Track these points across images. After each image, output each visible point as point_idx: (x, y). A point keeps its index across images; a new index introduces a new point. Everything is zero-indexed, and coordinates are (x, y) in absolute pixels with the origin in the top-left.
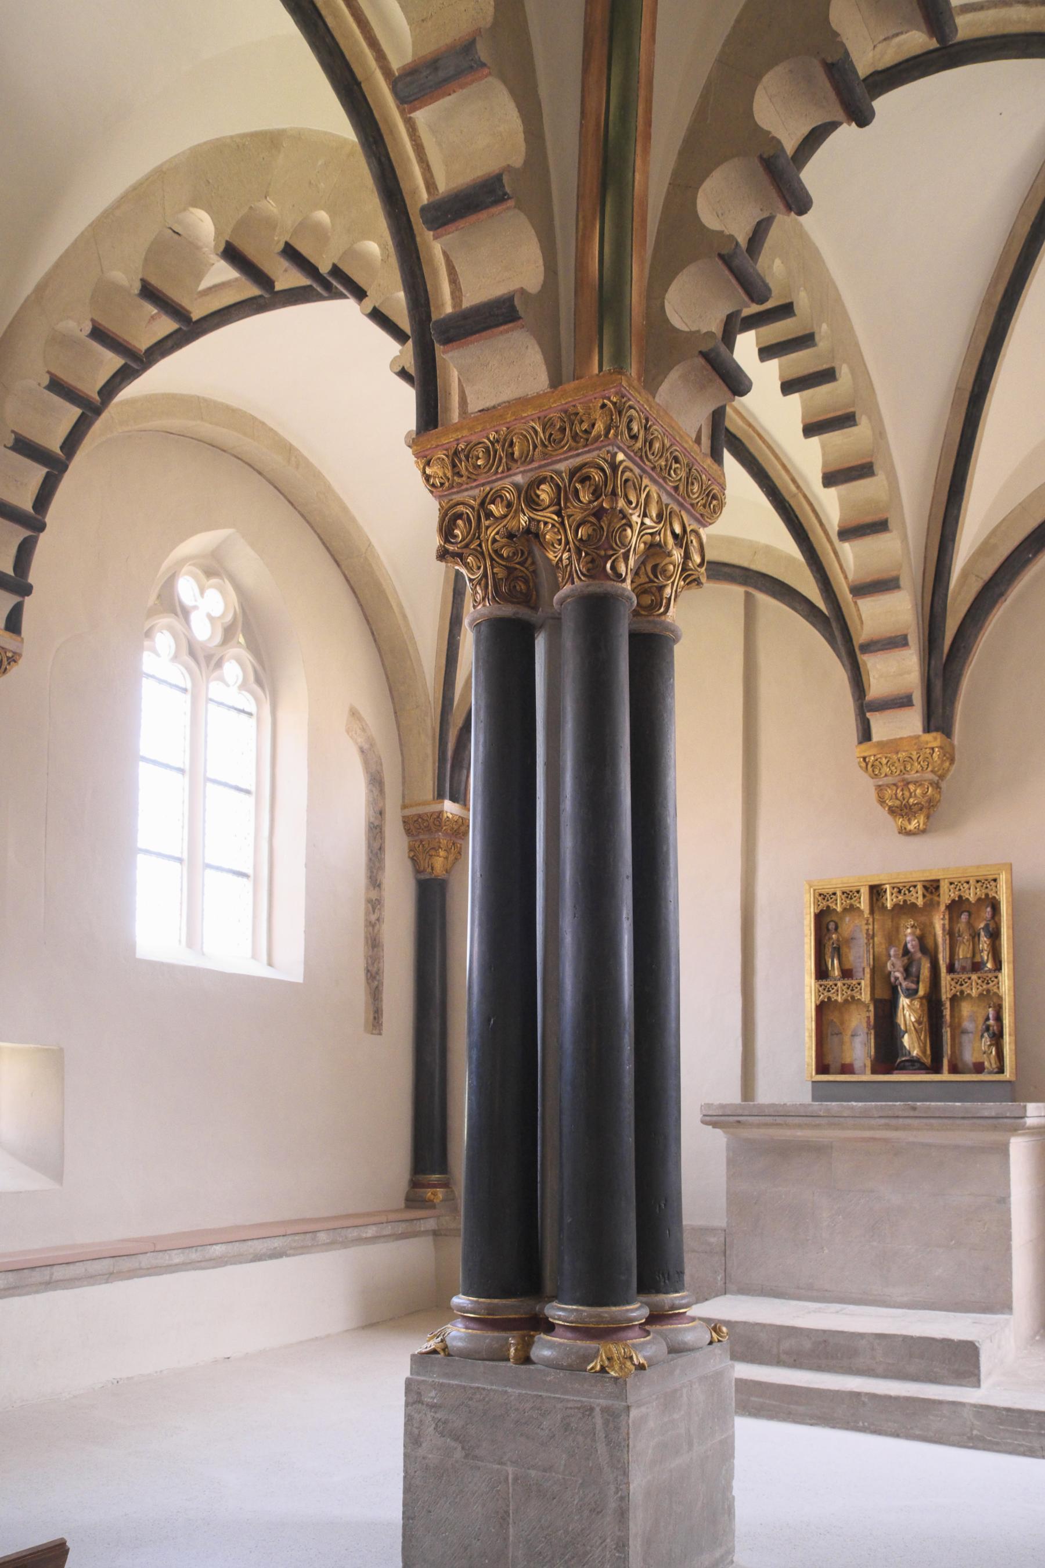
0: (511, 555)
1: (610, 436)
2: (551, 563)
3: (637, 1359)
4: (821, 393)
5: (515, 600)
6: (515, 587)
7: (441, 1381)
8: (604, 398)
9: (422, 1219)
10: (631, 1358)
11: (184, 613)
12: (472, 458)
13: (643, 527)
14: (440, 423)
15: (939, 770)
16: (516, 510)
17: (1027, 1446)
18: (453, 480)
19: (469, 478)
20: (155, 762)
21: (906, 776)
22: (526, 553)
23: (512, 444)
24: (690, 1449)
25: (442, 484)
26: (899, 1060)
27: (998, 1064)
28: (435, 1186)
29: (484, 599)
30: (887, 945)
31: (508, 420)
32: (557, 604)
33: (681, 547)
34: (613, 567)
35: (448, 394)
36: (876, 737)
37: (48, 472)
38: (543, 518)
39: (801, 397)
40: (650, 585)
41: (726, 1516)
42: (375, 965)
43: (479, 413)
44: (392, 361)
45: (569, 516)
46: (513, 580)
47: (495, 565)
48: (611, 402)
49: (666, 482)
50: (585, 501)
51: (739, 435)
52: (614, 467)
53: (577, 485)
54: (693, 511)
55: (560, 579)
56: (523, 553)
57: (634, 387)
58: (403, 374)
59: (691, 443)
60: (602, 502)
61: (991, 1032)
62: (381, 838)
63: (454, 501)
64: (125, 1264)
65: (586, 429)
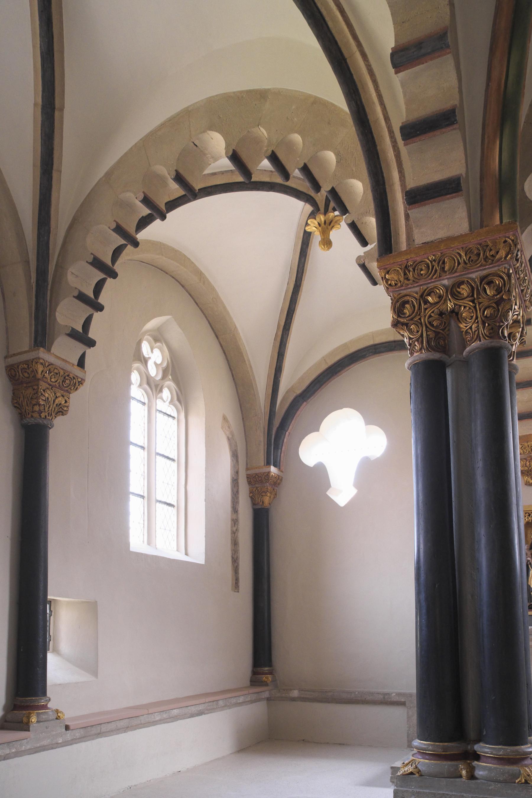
0: (438, 324)
1: (507, 258)
5: (439, 350)
6: (439, 343)
7: (418, 790)
8: (506, 237)
9: (263, 691)
11: (145, 361)
19: (414, 281)
22: (447, 324)
23: (444, 263)
25: (396, 284)
28: (266, 674)
29: (421, 349)
31: (442, 248)
38: (463, 304)
42: (236, 555)
43: (422, 245)
45: (480, 303)
46: (437, 339)
48: (510, 239)
60: (503, 296)
62: (237, 486)
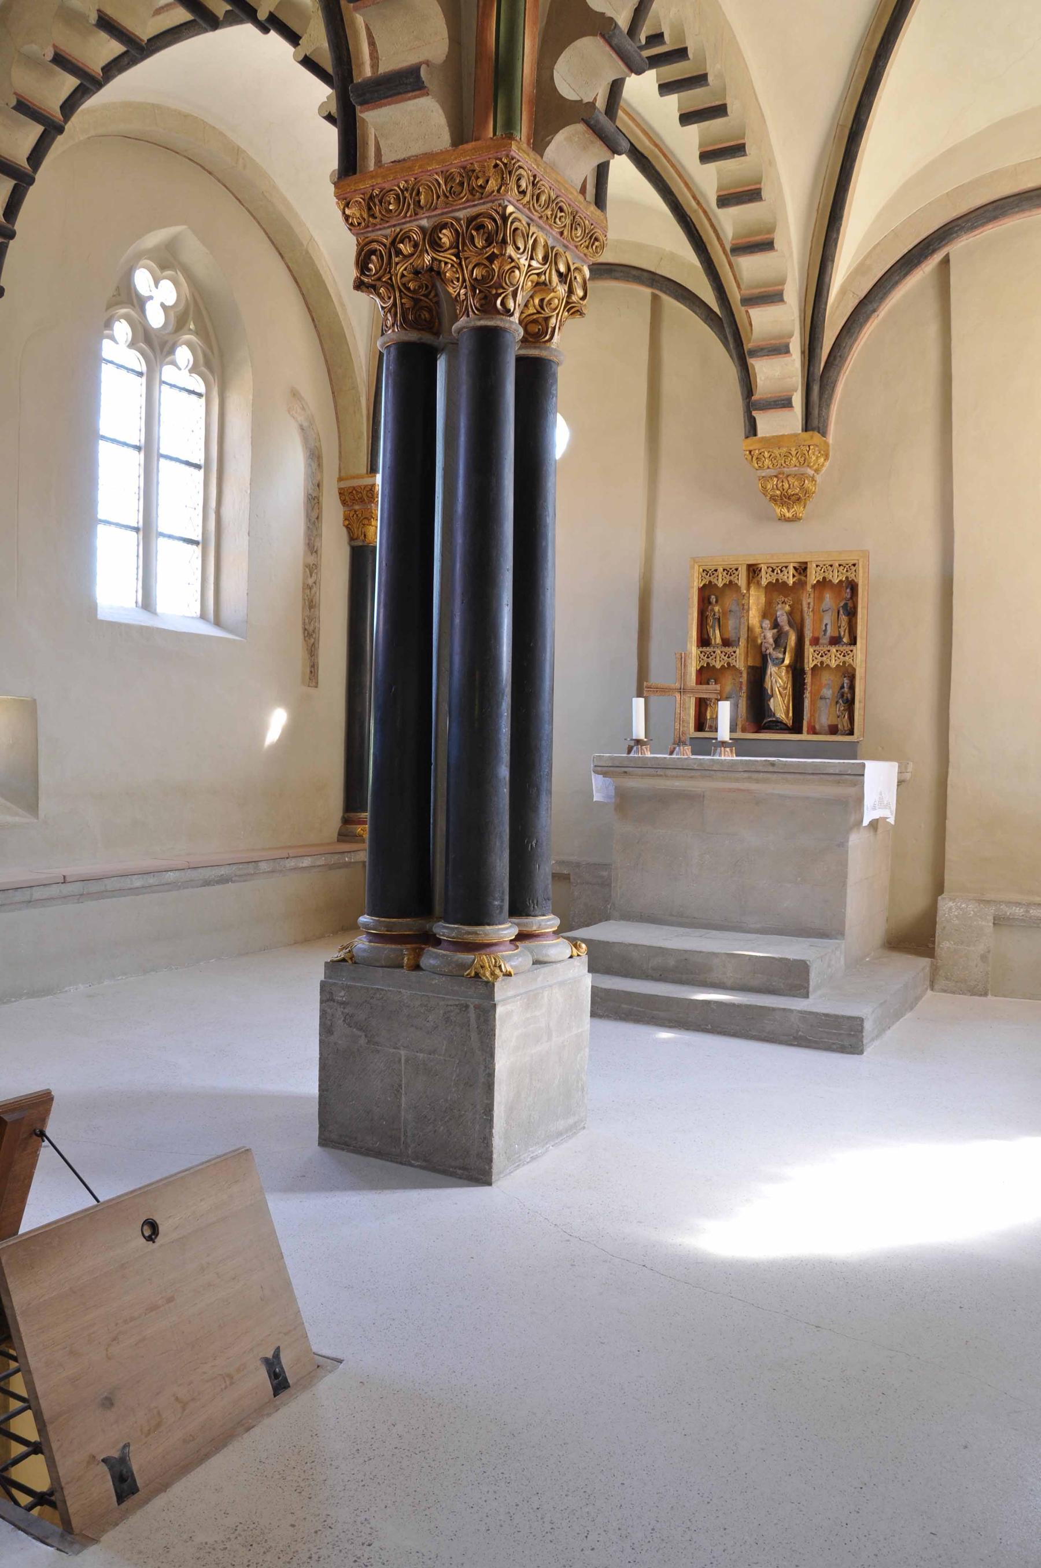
2: (452, 297)
3: (505, 967)
4: (715, 125)
6: (420, 315)
8: (497, 159)
10: (500, 967)
11: (139, 303)
12: (385, 203)
13: (530, 268)
14: (358, 170)
15: (814, 464)
16: (421, 250)
17: (839, 1044)
18: (369, 221)
19: (382, 219)
20: (114, 441)
21: (786, 470)
23: (418, 193)
24: (549, 1038)
25: (359, 224)
26: (765, 721)
27: (849, 726)
29: (393, 325)
30: (760, 618)
31: (416, 172)
32: (455, 332)
33: (565, 283)
34: (503, 303)
35: (365, 144)
36: (761, 433)
37: (16, 184)
38: (443, 259)
39: (698, 127)
40: (538, 316)
41: (580, 1093)
44: (320, 107)
45: (466, 259)
47: (403, 296)
48: (503, 162)
49: (552, 229)
50: (479, 247)
51: (646, 154)
52: (505, 218)
53: (473, 232)
54: (577, 251)
55: (458, 311)
56: (427, 287)
57: (523, 151)
58: (329, 118)
59: (575, 194)
61: (845, 698)
63: (369, 239)
64: (94, 887)
65: (481, 185)
